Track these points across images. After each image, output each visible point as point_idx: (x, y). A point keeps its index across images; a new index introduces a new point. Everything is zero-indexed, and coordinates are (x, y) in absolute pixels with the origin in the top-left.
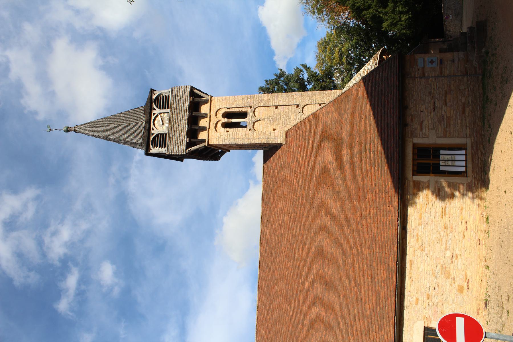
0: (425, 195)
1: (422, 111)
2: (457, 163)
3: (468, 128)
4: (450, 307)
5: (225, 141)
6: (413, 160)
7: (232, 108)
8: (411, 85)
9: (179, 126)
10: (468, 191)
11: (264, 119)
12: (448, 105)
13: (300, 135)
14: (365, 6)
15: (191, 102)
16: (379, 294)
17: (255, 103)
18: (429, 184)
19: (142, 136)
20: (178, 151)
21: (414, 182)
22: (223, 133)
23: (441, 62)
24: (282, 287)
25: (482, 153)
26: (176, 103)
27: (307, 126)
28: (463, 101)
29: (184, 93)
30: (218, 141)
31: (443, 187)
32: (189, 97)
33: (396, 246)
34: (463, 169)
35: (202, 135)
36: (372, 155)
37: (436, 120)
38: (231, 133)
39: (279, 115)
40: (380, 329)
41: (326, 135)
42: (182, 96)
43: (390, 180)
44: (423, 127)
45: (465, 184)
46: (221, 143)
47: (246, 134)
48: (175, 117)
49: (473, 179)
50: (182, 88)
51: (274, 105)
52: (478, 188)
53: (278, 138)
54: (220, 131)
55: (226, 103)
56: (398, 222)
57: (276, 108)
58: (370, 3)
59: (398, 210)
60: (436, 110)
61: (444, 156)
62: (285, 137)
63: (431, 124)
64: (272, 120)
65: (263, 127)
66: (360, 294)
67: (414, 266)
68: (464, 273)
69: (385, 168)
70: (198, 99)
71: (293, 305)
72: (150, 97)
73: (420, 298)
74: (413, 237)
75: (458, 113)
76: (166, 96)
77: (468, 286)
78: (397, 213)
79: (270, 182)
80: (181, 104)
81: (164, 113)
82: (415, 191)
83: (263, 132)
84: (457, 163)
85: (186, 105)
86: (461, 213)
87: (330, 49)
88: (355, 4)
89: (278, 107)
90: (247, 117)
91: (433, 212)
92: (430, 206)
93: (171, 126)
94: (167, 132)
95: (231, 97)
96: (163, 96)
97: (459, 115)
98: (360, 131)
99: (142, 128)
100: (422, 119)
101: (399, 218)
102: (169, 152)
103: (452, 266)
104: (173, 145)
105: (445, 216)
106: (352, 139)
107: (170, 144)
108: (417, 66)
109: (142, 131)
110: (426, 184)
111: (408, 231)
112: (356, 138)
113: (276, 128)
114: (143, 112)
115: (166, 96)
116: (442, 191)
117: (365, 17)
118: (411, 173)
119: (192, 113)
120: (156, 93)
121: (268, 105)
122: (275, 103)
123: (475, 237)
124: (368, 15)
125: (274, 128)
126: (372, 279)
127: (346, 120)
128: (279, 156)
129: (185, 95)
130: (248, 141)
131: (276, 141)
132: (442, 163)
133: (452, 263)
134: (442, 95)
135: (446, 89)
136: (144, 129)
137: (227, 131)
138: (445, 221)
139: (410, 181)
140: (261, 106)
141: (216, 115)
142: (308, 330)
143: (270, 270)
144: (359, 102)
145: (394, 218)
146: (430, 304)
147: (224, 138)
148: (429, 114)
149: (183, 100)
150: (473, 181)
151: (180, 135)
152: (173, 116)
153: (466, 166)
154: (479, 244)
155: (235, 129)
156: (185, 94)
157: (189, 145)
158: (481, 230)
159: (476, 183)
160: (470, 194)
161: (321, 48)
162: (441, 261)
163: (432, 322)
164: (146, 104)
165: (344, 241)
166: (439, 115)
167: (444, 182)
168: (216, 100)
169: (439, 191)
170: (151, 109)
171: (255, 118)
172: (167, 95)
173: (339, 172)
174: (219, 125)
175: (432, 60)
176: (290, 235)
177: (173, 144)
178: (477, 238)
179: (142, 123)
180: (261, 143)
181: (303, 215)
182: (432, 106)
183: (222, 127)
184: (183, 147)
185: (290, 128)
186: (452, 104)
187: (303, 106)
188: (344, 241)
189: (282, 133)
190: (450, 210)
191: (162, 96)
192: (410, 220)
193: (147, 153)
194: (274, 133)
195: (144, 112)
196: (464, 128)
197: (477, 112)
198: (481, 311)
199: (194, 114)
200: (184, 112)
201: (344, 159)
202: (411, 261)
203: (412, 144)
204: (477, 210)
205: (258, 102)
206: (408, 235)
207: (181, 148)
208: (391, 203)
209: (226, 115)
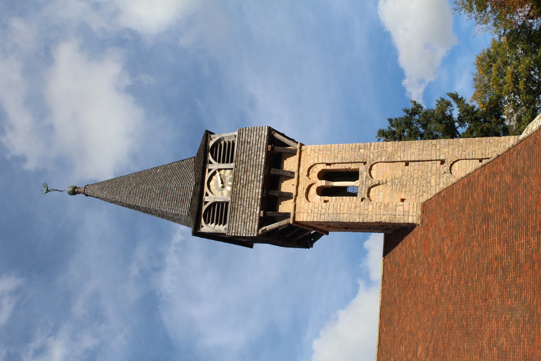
5: (322, 216)
7: (335, 163)
13: (446, 210)
15: (268, 153)
17: (371, 156)
19: (189, 205)
20: (245, 231)
22: (319, 204)
26: (245, 155)
29: (257, 138)
30: (309, 217)
35: (285, 207)
38: (332, 204)
41: (490, 211)
42: (254, 142)
47: (356, 207)
48: (242, 177)
51: (402, 160)
62: (420, 213)
65: (384, 195)
72: (204, 143)
79: (393, 286)
80: (253, 156)
83: (384, 204)
87: (498, 69)
90: (358, 179)
93: (236, 190)
94: (229, 199)
95: (332, 145)
99: (189, 192)
102: (231, 231)
104: (237, 221)
106: (537, 218)
107: (232, 218)
109: (190, 197)
113: (406, 198)
114: (192, 166)
119: (270, 171)
120: (214, 138)
121: (393, 160)
125: (403, 197)
127: (525, 186)
128: (410, 244)
129: (260, 142)
130: (360, 218)
137: (326, 201)
140: (382, 162)
141: (308, 175)
147: (319, 212)
149: (256, 149)
151: (250, 205)
152: (240, 174)
156: (260, 140)
157: (263, 222)
161: (483, 66)
168: (309, 150)
170: (206, 162)
171: (371, 181)
173: (512, 275)
174: (313, 190)
177: (238, 219)
179: (190, 183)
180: (380, 222)
184: (254, 224)
189: (415, 206)
191: (223, 141)
193: (197, 233)
194: (403, 206)
195: (195, 167)
199: (273, 171)
207: (251, 225)
209: (324, 175)
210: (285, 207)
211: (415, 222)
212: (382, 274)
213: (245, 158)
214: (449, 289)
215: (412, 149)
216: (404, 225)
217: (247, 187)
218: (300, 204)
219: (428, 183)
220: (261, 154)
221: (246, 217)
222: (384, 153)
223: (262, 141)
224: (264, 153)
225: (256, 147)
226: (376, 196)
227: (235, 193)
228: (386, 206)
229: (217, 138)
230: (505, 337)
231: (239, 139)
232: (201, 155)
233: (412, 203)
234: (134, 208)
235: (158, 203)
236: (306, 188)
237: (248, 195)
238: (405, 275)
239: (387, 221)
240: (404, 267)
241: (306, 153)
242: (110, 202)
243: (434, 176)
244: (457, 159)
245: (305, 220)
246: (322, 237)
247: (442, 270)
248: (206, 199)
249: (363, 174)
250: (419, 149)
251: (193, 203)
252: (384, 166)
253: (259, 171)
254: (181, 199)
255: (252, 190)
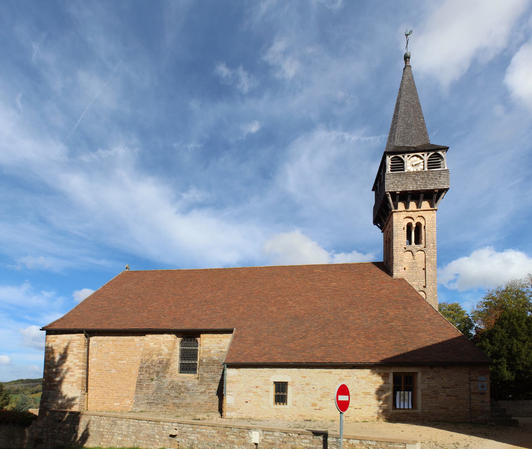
0: (379, 381)
1: (442, 379)
2: (402, 403)
3: (429, 411)
4: (302, 398)
5: (396, 227)
6: (405, 373)
7: (425, 231)
8: (464, 371)
9: (411, 182)
10: (383, 410)
11: (414, 259)
12: (447, 397)
13: (403, 290)
14: (494, 341)
15: (433, 190)
16: (304, 351)
17: (429, 250)
18: (387, 384)
19: (401, 146)
20: (388, 184)
21: (388, 373)
22: (403, 225)
23: (483, 394)
24: (282, 285)
25: (410, 419)
26: (433, 176)
27: (411, 294)
28: (450, 408)
29: (443, 182)
30: (396, 220)
31: (385, 393)
32: (438, 188)
33: (342, 362)
34: (398, 407)
35: (401, 206)
36: (403, 343)
37: (436, 389)
38: (403, 232)
39: (417, 272)
40: (280, 353)
41: (409, 309)
42: (440, 181)
43: (389, 356)
44: (430, 380)
45: (387, 408)
46: (394, 224)
47: (401, 245)
48: (419, 177)
49: (391, 413)
50: (447, 180)
51: (426, 266)
52: (385, 416)
53: (398, 272)
54: (404, 222)
55: (429, 225)
56: (360, 362)
57: (423, 269)
58: (497, 345)
59: (368, 362)
60: (443, 389)
61: (407, 394)
62: (399, 278)
63: (432, 385)
64: (413, 267)
65: (407, 259)
66: (298, 339)
67: (328, 374)
68: (325, 407)
69: (396, 353)
70: (436, 197)
71: (271, 293)
72: (441, 147)
73: (306, 379)
74: (348, 373)
75: (440, 404)
76: (441, 164)
77: (317, 409)
78: (366, 362)
79: (359, 269)
80: (432, 181)
81: (424, 165)
82: (382, 374)
83: (403, 260)
84: (402, 403)
85: (430, 186)
86: (367, 405)
87: (451, 314)
88: (497, 333)
89: (424, 271)
90: (416, 244)
91: (367, 387)
92: (371, 384)
93: (411, 174)
94: (406, 171)
95: (436, 228)
96: (440, 161)
97: (439, 405)
98: (419, 334)
99: (409, 144)
100: (436, 379)
101: (362, 363)
102: (388, 176)
103: (330, 399)
104: (393, 178)
105: (364, 395)
106: (411, 329)
107: (395, 175)
108: (480, 376)
109: (407, 145)
110: (387, 382)
111: (353, 370)
112: (412, 331)
113: (406, 270)
114: (425, 143)
115: (441, 164)
116: (382, 392)
117: (484, 341)
118: (395, 371)
119: (422, 193)
120: (444, 154)
121: (426, 262)
122: (428, 267)
123: (351, 414)
124: (485, 343)
125: (406, 269)
126: (312, 347)
127: (425, 324)
128: (381, 275)
129: (440, 184)
130: (395, 248)
131: (396, 271)
132: (402, 392)
133: (332, 399)
134: (455, 394)
135: (460, 396)
136: (408, 147)
137: (404, 228)
138: (360, 394)
139: (389, 371)
140: (425, 256)
141: (419, 216)
142: (258, 305)
143: (291, 275)
144: (442, 333)
145: (361, 360)
146: (303, 385)
147: (398, 226)
148: (440, 384)
149: (436, 183)
150: (390, 413)
151: (403, 185)
152: (421, 175)
153: (400, 409)
154: (346, 417)
155: (406, 235)
156: (441, 184)
157: (393, 194)
158: (355, 417)
159: (389, 415)
160: (381, 411)
161: (453, 307)
162: (333, 392)
163: (291, 387)
164: (432, 145)
165: (332, 326)
166: (439, 391)
167: (390, 393)
168: (433, 215)
169: (382, 391)
170: (428, 151)
171: (415, 252)
172: (442, 165)
173: (382, 320)
174: (410, 220)
175: (484, 387)
176: (322, 288)
177: (395, 178)
178: (350, 415)
179: (415, 143)
180: (393, 259)
181: (341, 296)
182: (446, 386)
183: (408, 223)
184: (392, 189)
185: (407, 281)
186: (448, 401)
187: (425, 291)
188: (332, 326)
189: (402, 275)
190: (369, 398)
191: (441, 160)
192: (360, 371)
193: (386, 154)
194: (402, 269)
195: (425, 144)
196: (429, 408)
197: (441, 417)
198: (301, 417)
199: (422, 195)
200: (424, 185)
201: (393, 324)
202: (331, 372)
203: (417, 372)
204: (369, 416)
205: (429, 252)
206: (350, 370)
207: (391, 187)
208: (371, 357)
209: (419, 225)
210: (401, 206)
211: (394, 276)
212: (363, 263)
213: (431, 176)
214: (366, 294)
215: (432, 271)
216: (391, 271)
217: (413, 181)
218: (402, 214)
219: (414, 281)
220: (433, 186)
221: (396, 183)
222: (430, 257)
223: (441, 186)
224: (433, 188)
225: (437, 182)
226: (407, 255)
227: (410, 174)
228: (402, 261)
229: (443, 156)
230: (353, 319)
231: (443, 170)
232: (433, 147)
233: (403, 273)
234: (397, 108)
235: (401, 124)
236: (411, 216)
237: (408, 183)
238: (366, 274)
239: (394, 262)
240: (370, 273)
241: (432, 214)
242: (400, 89)
243: (417, 283)
244: (426, 294)
245: (394, 218)
246: (380, 229)
247: (373, 290)
248: (406, 156)
249: (419, 247)
250: (432, 275)
251: (403, 148)
252: (423, 258)
253: (423, 187)
254: (405, 139)
255: (411, 184)
